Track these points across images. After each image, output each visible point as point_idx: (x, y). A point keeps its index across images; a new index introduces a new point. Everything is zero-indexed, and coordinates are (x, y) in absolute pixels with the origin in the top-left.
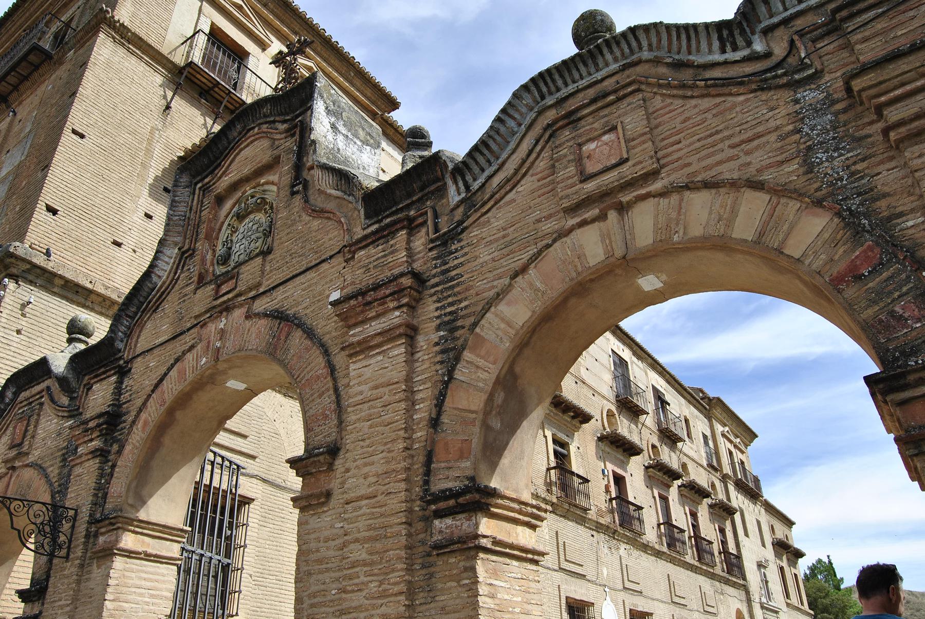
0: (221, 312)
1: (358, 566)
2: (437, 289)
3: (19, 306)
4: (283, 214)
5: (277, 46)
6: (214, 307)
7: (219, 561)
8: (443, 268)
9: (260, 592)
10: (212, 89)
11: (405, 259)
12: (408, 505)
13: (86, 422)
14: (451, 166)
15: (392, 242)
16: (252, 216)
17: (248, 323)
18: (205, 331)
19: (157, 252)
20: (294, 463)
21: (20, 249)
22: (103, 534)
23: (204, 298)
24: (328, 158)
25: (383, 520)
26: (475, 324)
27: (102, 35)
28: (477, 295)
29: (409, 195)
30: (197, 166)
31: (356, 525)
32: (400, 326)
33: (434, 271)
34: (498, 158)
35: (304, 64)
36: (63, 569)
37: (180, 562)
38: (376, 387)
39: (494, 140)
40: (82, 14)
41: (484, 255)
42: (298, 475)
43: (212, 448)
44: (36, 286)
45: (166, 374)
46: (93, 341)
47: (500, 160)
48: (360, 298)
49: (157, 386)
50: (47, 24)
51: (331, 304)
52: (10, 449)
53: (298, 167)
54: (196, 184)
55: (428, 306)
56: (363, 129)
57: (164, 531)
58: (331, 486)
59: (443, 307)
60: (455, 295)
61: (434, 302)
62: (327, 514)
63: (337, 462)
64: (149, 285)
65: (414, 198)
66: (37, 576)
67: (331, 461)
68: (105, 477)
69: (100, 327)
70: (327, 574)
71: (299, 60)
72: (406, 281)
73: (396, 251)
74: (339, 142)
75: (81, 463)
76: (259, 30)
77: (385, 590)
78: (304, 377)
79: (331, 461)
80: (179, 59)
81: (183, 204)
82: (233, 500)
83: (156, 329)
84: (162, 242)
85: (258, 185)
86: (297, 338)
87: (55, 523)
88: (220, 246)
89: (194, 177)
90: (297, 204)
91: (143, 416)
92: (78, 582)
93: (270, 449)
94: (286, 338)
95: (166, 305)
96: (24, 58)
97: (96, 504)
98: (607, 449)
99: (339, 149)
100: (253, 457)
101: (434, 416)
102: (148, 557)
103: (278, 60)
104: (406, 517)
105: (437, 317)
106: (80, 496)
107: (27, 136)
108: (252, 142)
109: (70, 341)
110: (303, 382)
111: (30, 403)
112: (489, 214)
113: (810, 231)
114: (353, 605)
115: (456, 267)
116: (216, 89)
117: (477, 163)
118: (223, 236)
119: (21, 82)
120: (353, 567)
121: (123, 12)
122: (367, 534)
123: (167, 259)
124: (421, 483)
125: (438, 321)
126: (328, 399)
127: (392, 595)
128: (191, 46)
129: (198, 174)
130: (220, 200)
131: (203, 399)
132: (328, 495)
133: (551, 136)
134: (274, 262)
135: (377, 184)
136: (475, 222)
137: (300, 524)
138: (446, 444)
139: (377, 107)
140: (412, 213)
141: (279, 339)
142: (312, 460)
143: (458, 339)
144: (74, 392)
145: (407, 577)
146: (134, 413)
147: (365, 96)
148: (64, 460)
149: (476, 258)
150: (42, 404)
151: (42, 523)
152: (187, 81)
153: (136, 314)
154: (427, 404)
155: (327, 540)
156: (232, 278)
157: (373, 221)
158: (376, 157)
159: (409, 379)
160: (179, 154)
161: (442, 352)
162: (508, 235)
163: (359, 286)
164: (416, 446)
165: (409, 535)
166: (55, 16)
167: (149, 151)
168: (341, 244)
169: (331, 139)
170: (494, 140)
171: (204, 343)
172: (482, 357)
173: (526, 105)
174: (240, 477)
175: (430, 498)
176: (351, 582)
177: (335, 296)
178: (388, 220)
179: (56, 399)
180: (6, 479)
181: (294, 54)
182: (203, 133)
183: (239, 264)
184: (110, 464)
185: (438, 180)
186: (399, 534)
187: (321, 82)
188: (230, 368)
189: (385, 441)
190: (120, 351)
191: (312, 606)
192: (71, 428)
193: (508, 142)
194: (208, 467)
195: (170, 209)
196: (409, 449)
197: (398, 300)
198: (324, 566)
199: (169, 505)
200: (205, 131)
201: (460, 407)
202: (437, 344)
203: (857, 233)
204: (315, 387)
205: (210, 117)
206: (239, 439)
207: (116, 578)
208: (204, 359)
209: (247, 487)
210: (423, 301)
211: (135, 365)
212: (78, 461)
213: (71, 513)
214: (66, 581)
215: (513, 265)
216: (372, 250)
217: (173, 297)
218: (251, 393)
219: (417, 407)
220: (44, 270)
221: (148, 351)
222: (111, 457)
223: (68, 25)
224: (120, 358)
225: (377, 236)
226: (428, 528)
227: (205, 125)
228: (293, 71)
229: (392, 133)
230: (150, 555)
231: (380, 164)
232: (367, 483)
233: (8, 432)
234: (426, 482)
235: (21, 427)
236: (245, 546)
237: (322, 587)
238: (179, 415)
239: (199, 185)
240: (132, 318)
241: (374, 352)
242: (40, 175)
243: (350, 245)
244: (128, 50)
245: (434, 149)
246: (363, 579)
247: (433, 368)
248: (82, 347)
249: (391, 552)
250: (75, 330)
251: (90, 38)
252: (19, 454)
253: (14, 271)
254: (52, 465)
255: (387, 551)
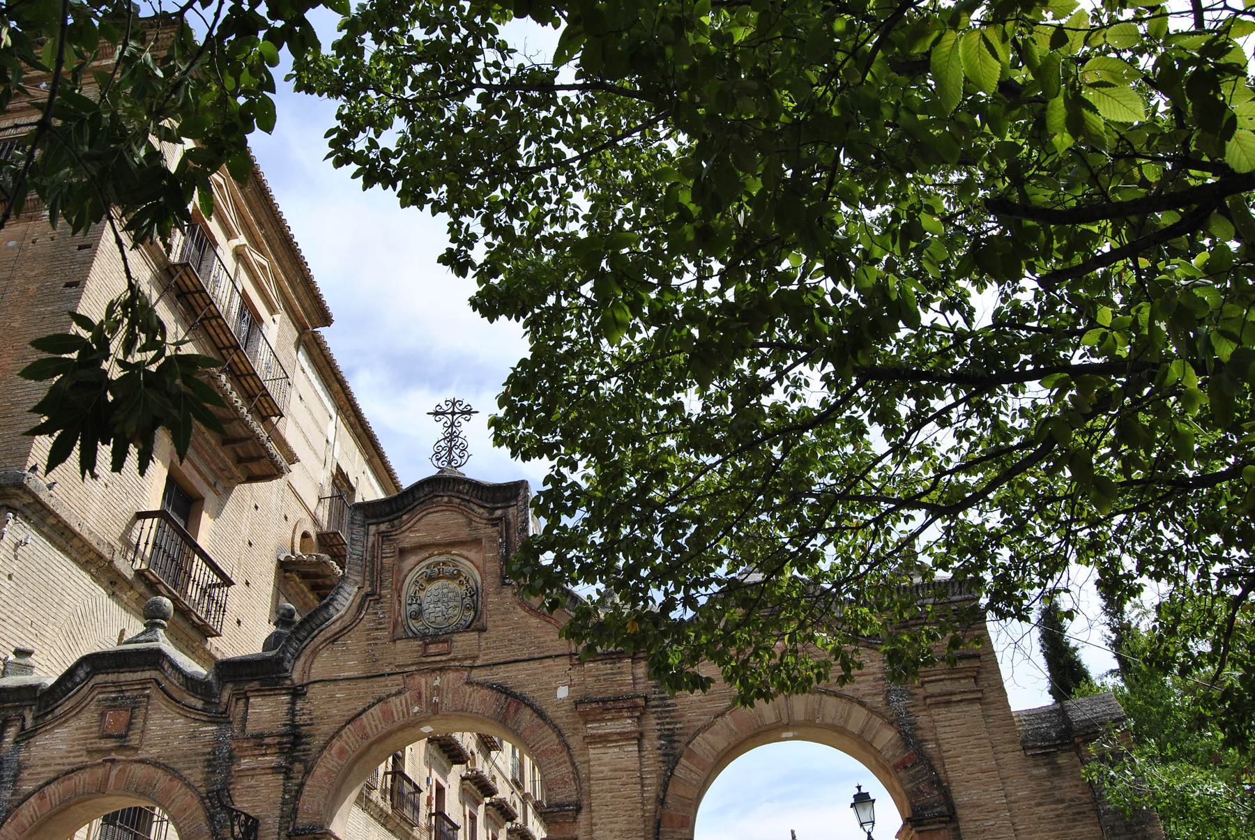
17: (468, 689)
26: (689, 742)
38: (615, 770)
59: (662, 724)
72: (641, 702)
98: (435, 754)
113: (886, 737)
147: (302, 307)
153: (306, 638)
161: (664, 755)
203: (907, 744)
220: (44, 506)
240: (302, 642)
253: (17, 504)
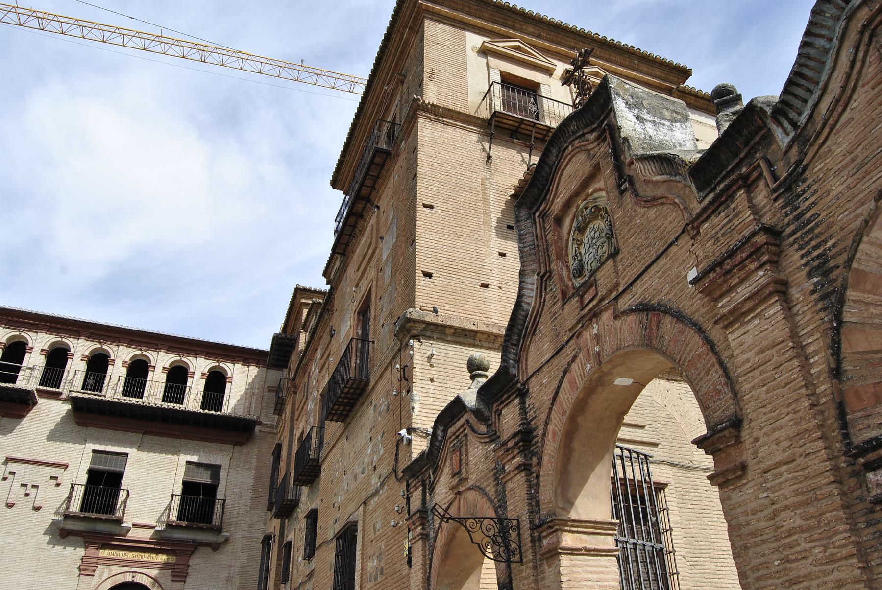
0: (591, 320)
1: (795, 534)
2: (795, 236)
3: (426, 360)
4: (619, 214)
5: (561, 67)
6: (584, 317)
7: (653, 547)
8: (795, 213)
9: (697, 572)
10: (519, 127)
11: (752, 217)
12: (832, 463)
13: (505, 443)
14: (769, 110)
15: (732, 206)
16: (591, 226)
17: (618, 323)
18: (581, 340)
19: (520, 283)
20: (700, 442)
21: (414, 313)
22: (545, 537)
23: (571, 311)
24: (644, 149)
25: (809, 482)
26: (850, 260)
27: (420, 120)
28: (842, 229)
29: (735, 154)
30: (530, 197)
31: (780, 492)
32: (767, 285)
33: (787, 220)
34: (818, 83)
35: (593, 72)
36: (521, 572)
37: (617, 553)
38: (762, 351)
39: (807, 66)
40: (401, 109)
41: (837, 186)
42: (707, 453)
43: (617, 444)
44: (434, 340)
45: (559, 387)
46: (491, 373)
47: (821, 84)
48: (718, 269)
49: (554, 399)
50: (379, 130)
51: (691, 283)
52: (452, 477)
53: (619, 167)
54: (534, 214)
55: (791, 256)
56: (667, 109)
57: (596, 527)
58: (744, 457)
59: (809, 253)
60: (817, 237)
61: (797, 250)
62: (748, 486)
63: (743, 434)
64: (523, 313)
65: (742, 155)
66: (502, 580)
67: (736, 433)
68: (534, 487)
69: (493, 360)
70: (764, 546)
71: (587, 70)
73: (740, 212)
74: (649, 130)
75: (511, 479)
76: (541, 60)
77: (832, 555)
78: (685, 359)
79: (736, 433)
80: (485, 114)
81: (529, 235)
82: (650, 488)
83: (539, 350)
84: (522, 274)
85: (588, 196)
86: (668, 324)
87: (504, 534)
88: (571, 261)
89: (531, 208)
90: (629, 200)
91: (551, 428)
92: (536, 581)
93: (669, 433)
94: (658, 326)
95: (541, 327)
96: (372, 162)
97: (532, 512)
99: (650, 137)
100: (655, 445)
101: (833, 365)
102: (589, 552)
103: (567, 79)
104: (833, 475)
105: (805, 265)
106: (517, 507)
107: (391, 223)
108: (570, 160)
109: (473, 378)
110: (686, 364)
111: (457, 437)
112: (828, 143)
114: (802, 573)
115: (809, 208)
116: (523, 126)
117: (796, 96)
118: (571, 252)
119: (375, 182)
120: (790, 535)
121: (430, 94)
122: (796, 499)
123: (530, 287)
124: (840, 437)
125: (808, 269)
126: (716, 374)
127: (841, 559)
128: (490, 99)
129: (534, 204)
130: (559, 221)
131: (598, 401)
132: (744, 467)
133: (871, 37)
134: (625, 260)
135: (700, 155)
136: (814, 156)
137: (723, 501)
138: (857, 392)
139: (670, 82)
140: (744, 170)
141: (651, 330)
142: (717, 436)
143: (836, 280)
144: (489, 419)
145: (853, 538)
146: (542, 427)
147: (655, 77)
148: (496, 479)
149: (828, 192)
150: (466, 436)
151: (494, 535)
152: (499, 129)
153: (519, 341)
154: (822, 354)
155: (754, 512)
156: (591, 286)
157: (706, 192)
158: (689, 130)
159: (794, 335)
160: (510, 194)
161: (822, 298)
162: (857, 157)
163: (713, 258)
164: (823, 400)
165: (843, 494)
166: (383, 120)
167: (486, 200)
168: (682, 224)
169: (641, 130)
170: (807, 66)
171: (584, 351)
172: (869, 292)
173: (831, 17)
174: (651, 466)
175: (855, 452)
176: (793, 551)
177: (692, 274)
178: (722, 186)
179: (476, 428)
180: (456, 502)
181: (580, 67)
182: (524, 168)
183: (594, 272)
184: (534, 475)
185: (760, 129)
186: (830, 495)
187: (614, 82)
188: (614, 368)
189: (787, 402)
190: (515, 376)
191: (758, 579)
192: (495, 451)
193: (824, 63)
194: (619, 462)
195: (520, 243)
196: (816, 406)
197: (758, 259)
198: (759, 538)
199: (593, 502)
200: (525, 165)
201: (861, 350)
202: (813, 292)
204: (699, 365)
205: (525, 151)
206: (637, 430)
207: (567, 575)
208: (589, 365)
209: (659, 474)
210: (784, 254)
211: (531, 385)
212: (508, 478)
213: (515, 523)
214: (526, 582)
215: (873, 187)
216: (715, 220)
217: (545, 317)
218: (639, 386)
219: (812, 361)
220: (436, 325)
221: (538, 370)
222: (534, 469)
223: (393, 123)
224: (517, 382)
225: (716, 204)
226: (862, 483)
227: (523, 160)
228: (585, 83)
229: (700, 103)
230: (590, 550)
231: (696, 135)
232: (780, 448)
233: (448, 464)
234: (846, 436)
235: (456, 458)
236: (671, 530)
237: (763, 559)
238: (580, 420)
239: (537, 214)
240: (517, 345)
241: (749, 318)
242: (410, 249)
243: (692, 222)
244: (443, 123)
245: (745, 102)
246: (804, 546)
247: (817, 317)
248: (483, 380)
249: (828, 515)
250: (475, 368)
251: (413, 126)
252: (461, 480)
253: (415, 332)
254: (488, 485)
255: (823, 513)
